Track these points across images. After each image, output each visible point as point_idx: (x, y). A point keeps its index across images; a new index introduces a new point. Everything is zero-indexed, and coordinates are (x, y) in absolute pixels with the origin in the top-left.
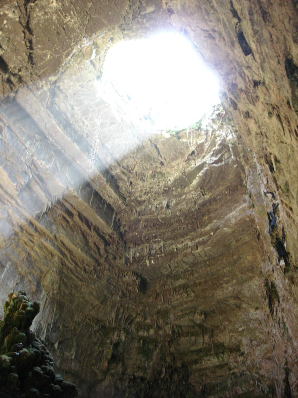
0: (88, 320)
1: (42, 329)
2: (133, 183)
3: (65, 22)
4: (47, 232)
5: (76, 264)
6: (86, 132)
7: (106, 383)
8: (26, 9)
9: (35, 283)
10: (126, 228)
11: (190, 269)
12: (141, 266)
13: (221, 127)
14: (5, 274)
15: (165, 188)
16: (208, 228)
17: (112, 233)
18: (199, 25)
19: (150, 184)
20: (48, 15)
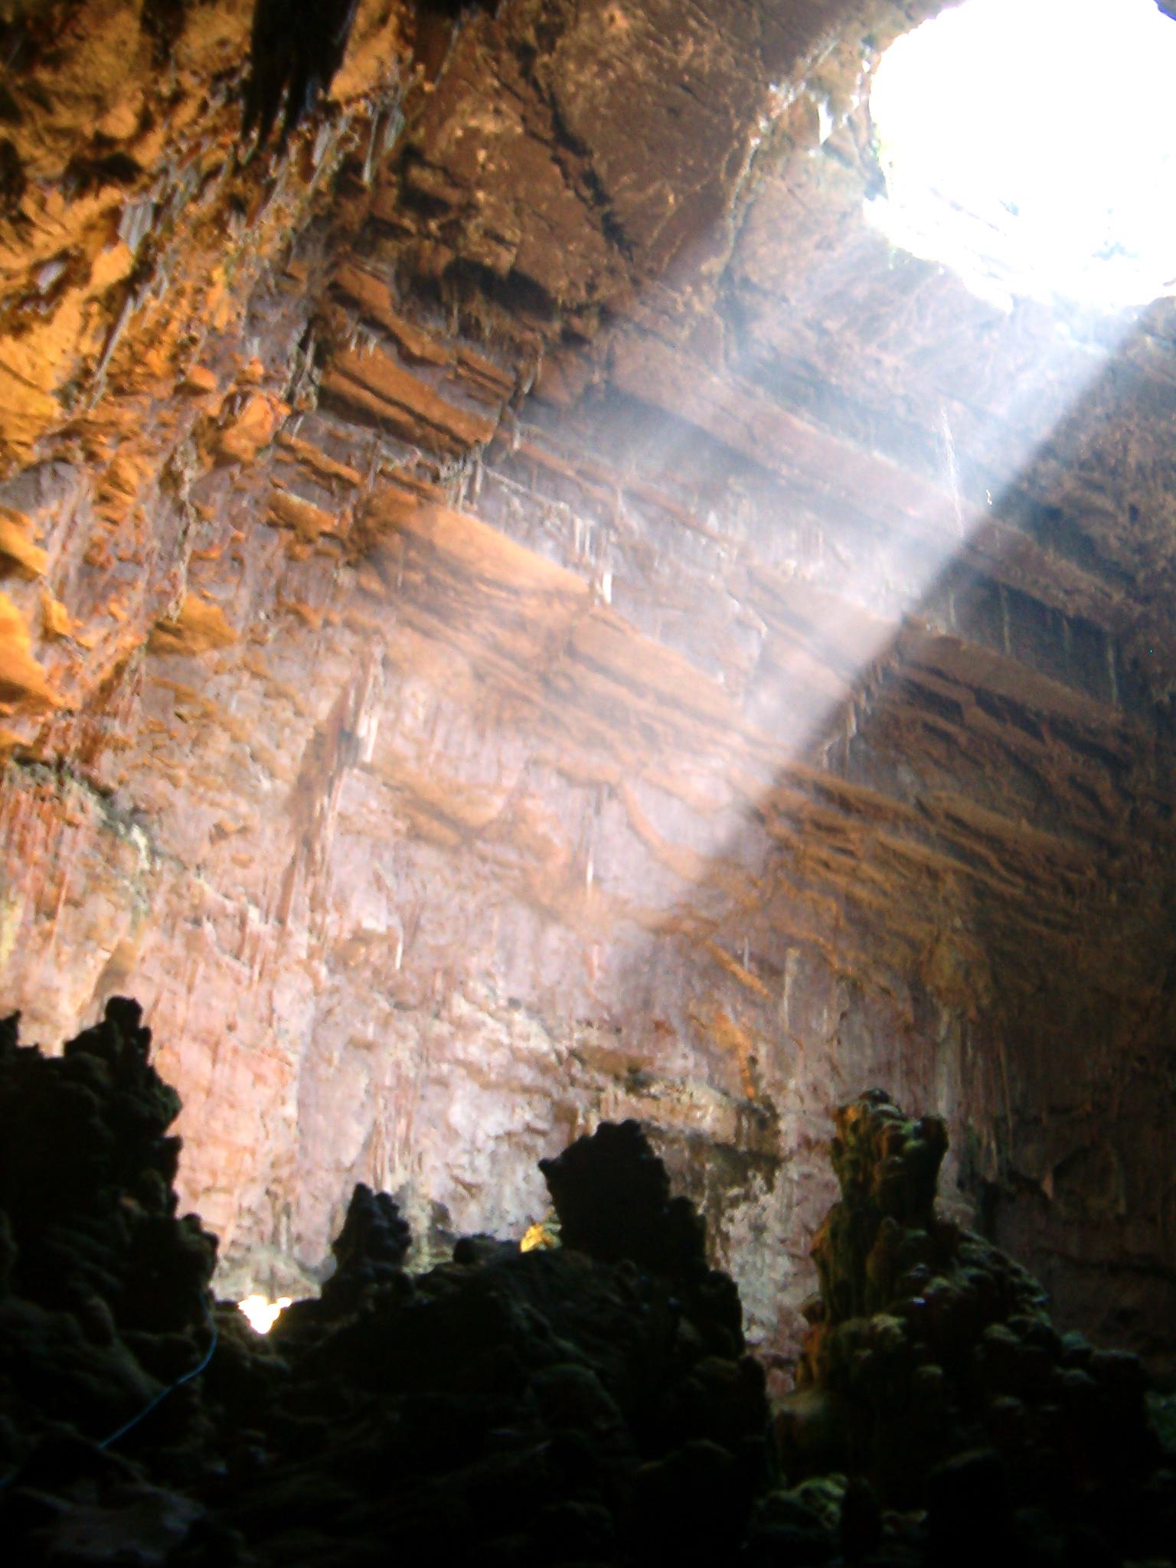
0: (1137, 1065)
1: (980, 1143)
2: (1142, 509)
4: (888, 801)
5: (1030, 878)
6: (901, 391)
8: (535, 84)
9: (906, 992)
14: (792, 997)
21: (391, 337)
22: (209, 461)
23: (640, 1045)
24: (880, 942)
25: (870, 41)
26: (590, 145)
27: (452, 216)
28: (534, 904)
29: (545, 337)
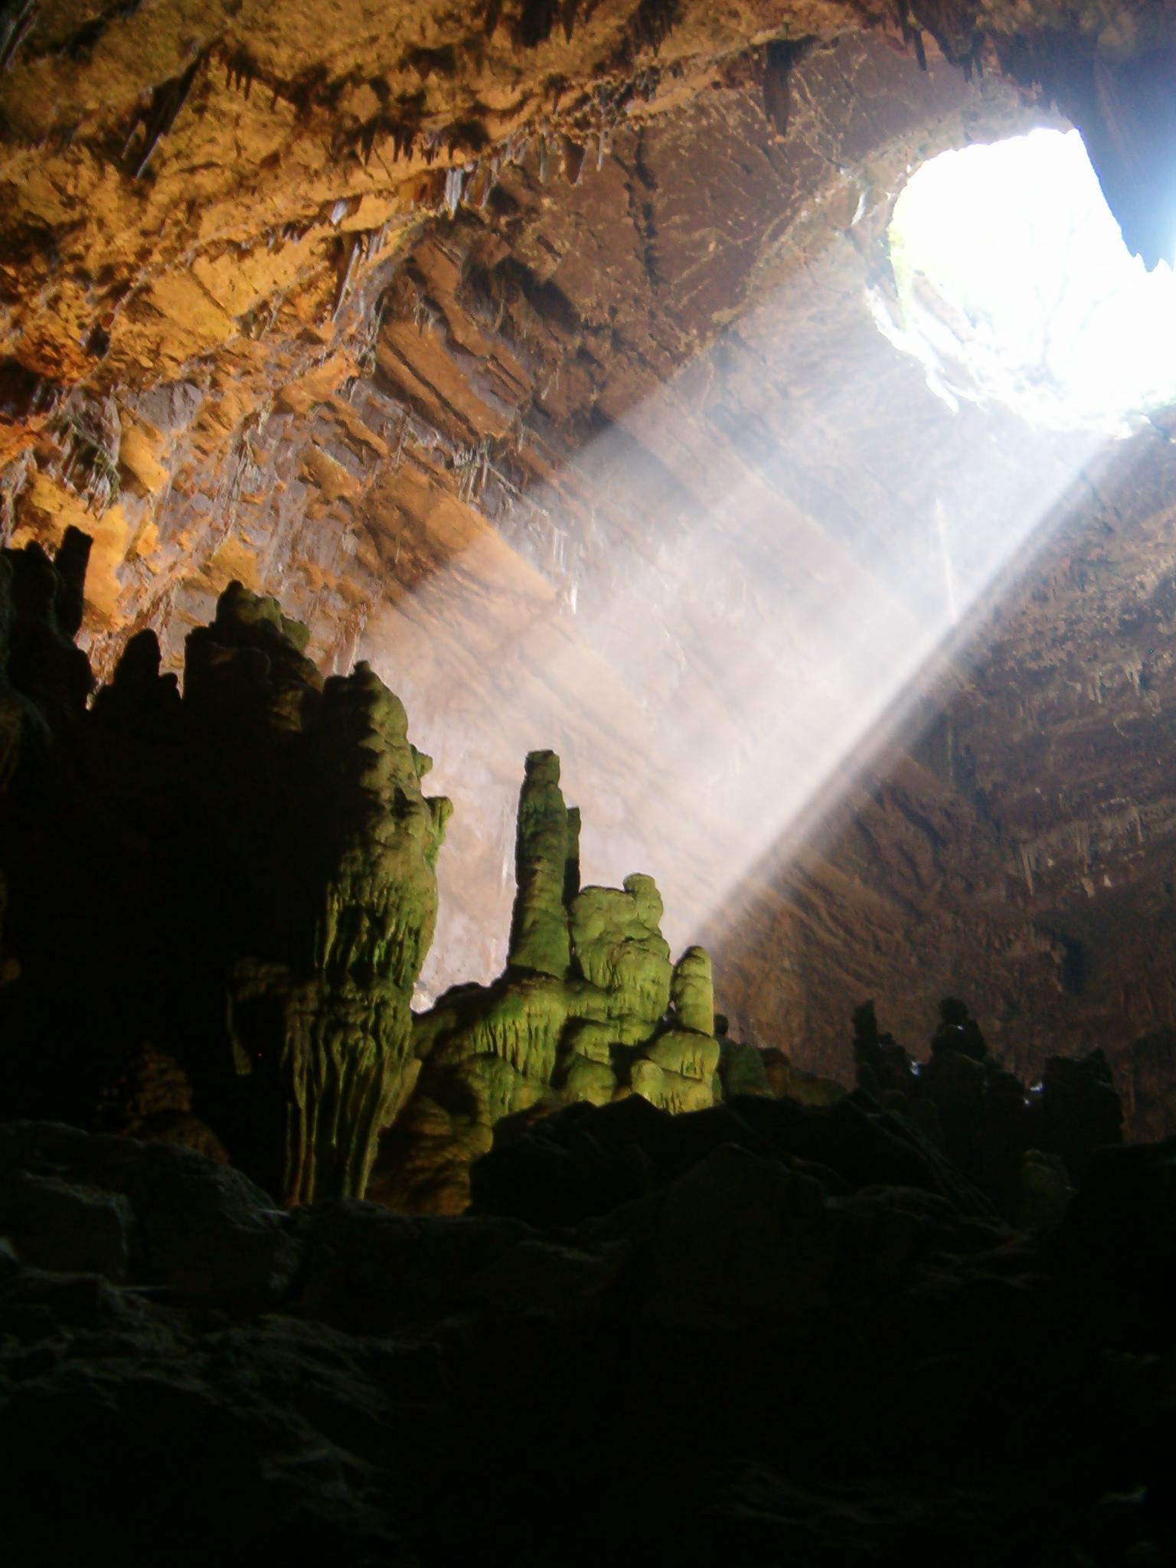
5: (849, 931)
15: (1126, 617)
19: (1071, 608)
26: (658, 180)
27: (518, 215)
29: (565, 349)
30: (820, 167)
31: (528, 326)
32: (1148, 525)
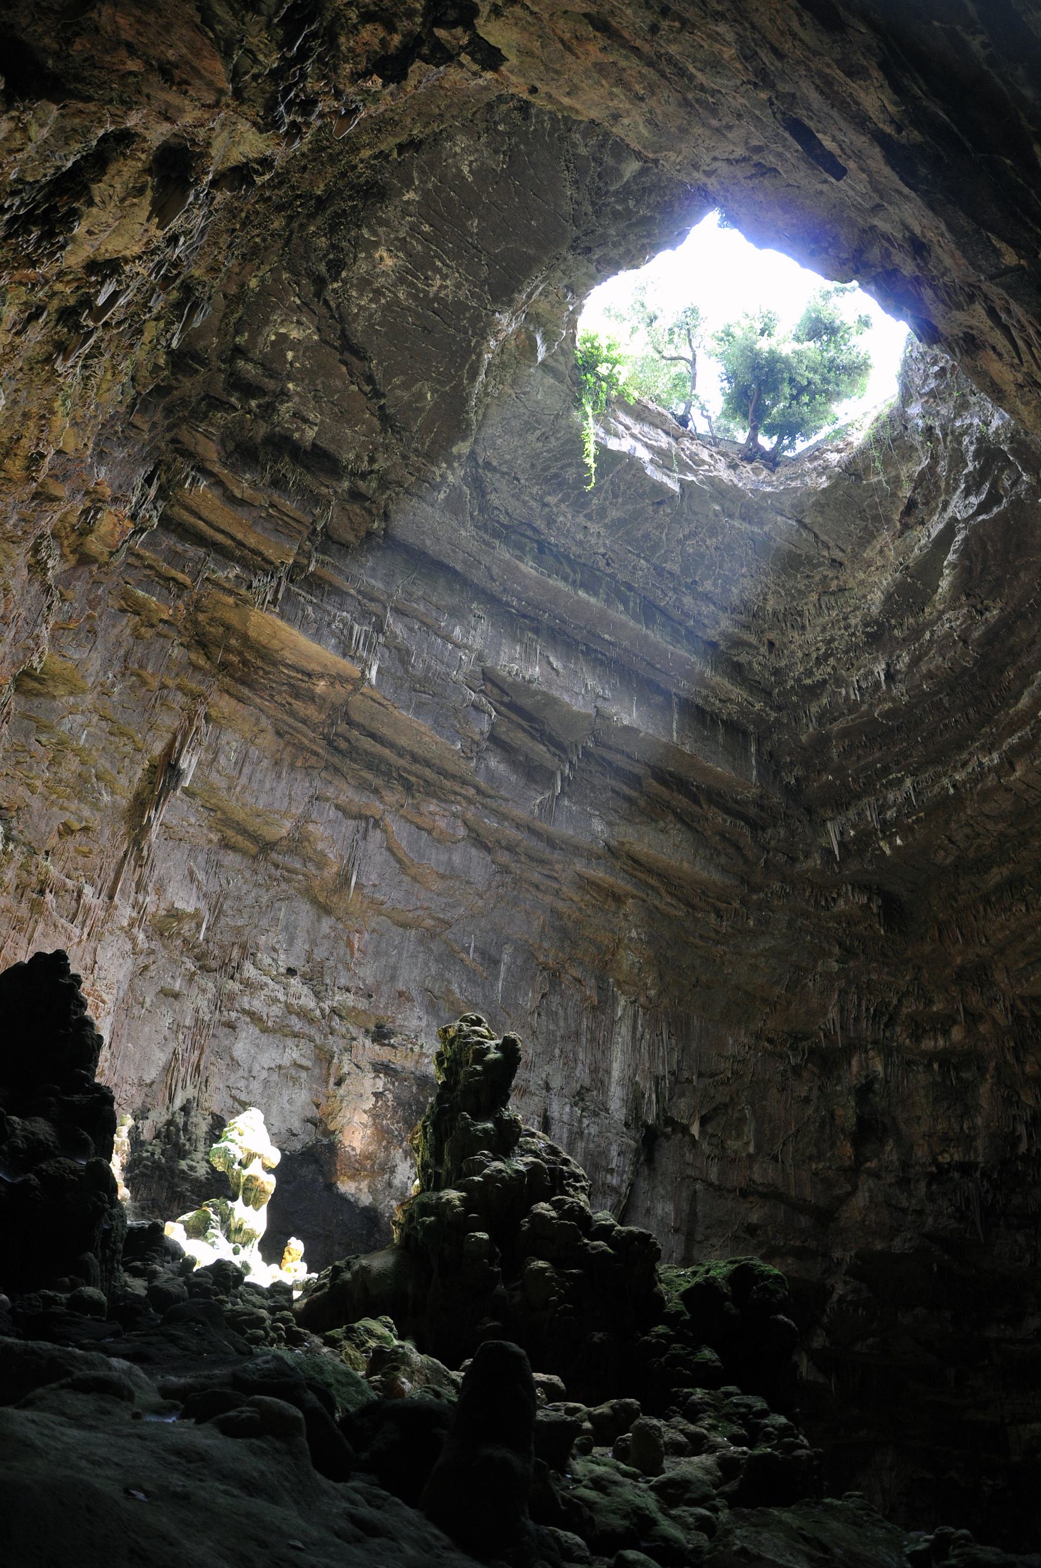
3: (431, 295)
5: (689, 904)
6: (602, 550)
7: (861, 1199)
8: (326, 303)
9: (593, 982)
10: (798, 771)
11: (1012, 831)
12: (870, 861)
13: (963, 406)
16: (1025, 701)
17: (761, 797)
18: (716, 154)
20: (384, 296)
21: (218, 483)
22: (73, 559)
23: (386, 1008)
24: (574, 944)
25: (570, 288)
28: (314, 901)
30: (480, 316)
31: (294, 476)
32: (868, 554)
